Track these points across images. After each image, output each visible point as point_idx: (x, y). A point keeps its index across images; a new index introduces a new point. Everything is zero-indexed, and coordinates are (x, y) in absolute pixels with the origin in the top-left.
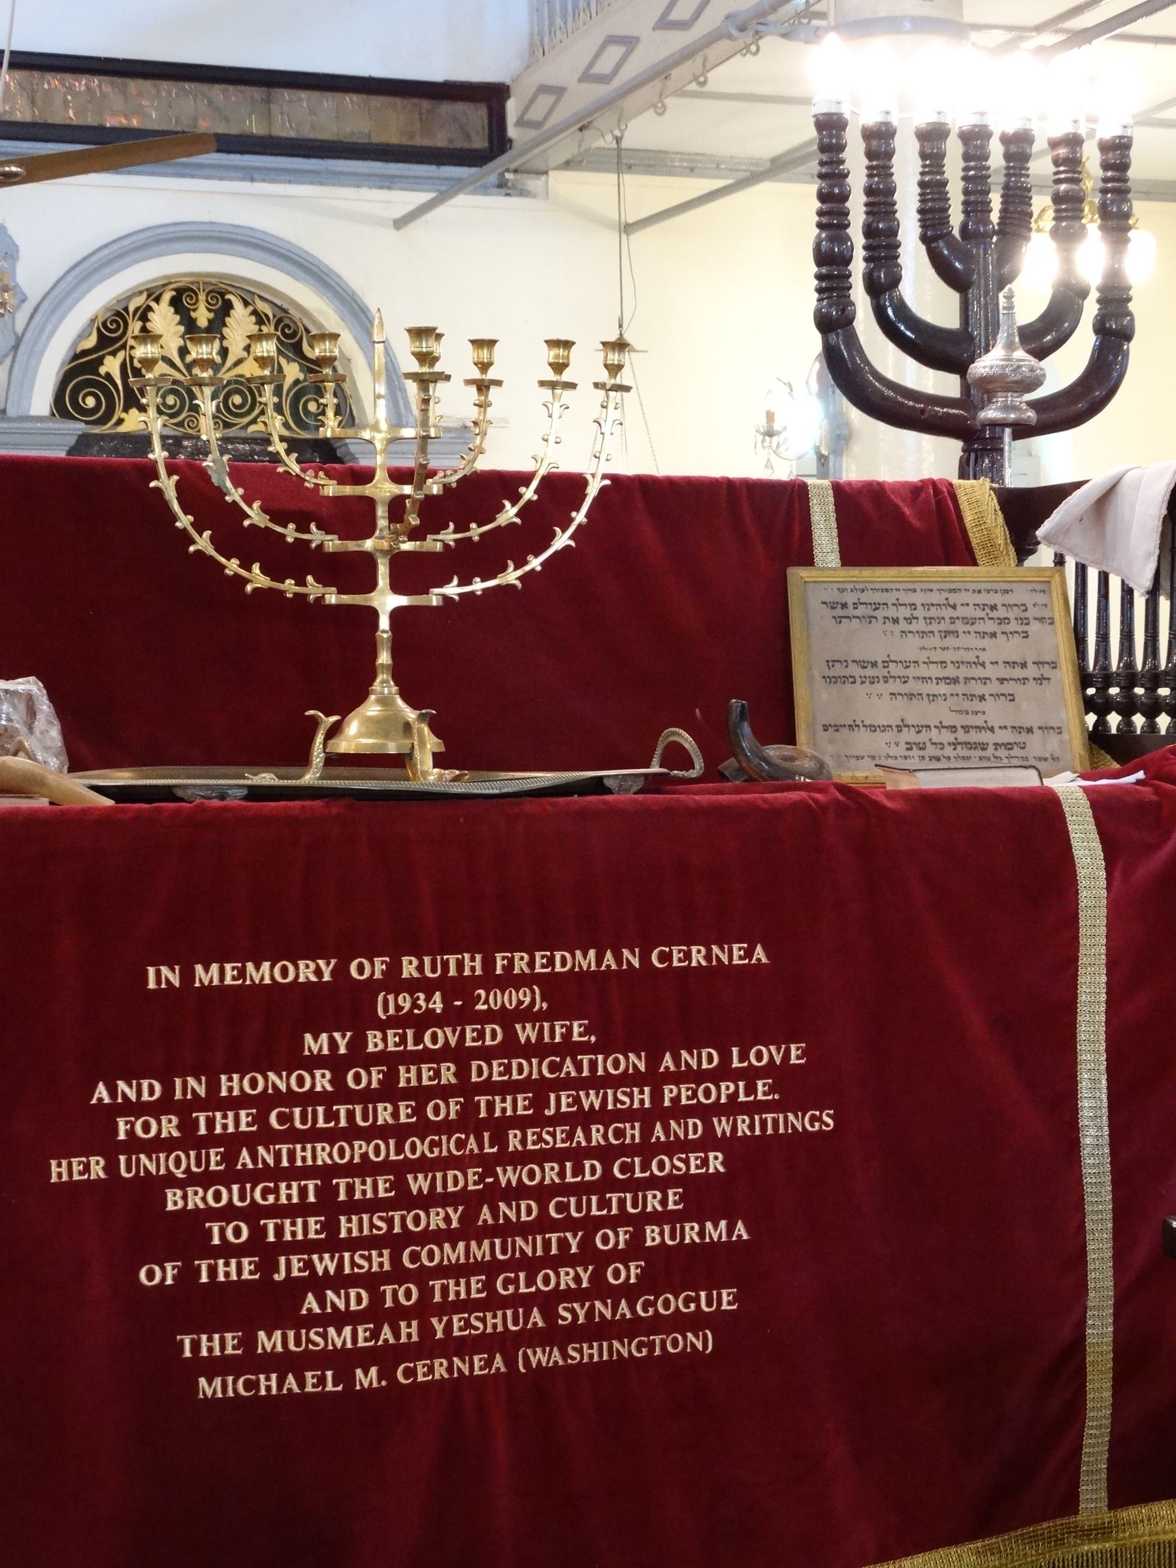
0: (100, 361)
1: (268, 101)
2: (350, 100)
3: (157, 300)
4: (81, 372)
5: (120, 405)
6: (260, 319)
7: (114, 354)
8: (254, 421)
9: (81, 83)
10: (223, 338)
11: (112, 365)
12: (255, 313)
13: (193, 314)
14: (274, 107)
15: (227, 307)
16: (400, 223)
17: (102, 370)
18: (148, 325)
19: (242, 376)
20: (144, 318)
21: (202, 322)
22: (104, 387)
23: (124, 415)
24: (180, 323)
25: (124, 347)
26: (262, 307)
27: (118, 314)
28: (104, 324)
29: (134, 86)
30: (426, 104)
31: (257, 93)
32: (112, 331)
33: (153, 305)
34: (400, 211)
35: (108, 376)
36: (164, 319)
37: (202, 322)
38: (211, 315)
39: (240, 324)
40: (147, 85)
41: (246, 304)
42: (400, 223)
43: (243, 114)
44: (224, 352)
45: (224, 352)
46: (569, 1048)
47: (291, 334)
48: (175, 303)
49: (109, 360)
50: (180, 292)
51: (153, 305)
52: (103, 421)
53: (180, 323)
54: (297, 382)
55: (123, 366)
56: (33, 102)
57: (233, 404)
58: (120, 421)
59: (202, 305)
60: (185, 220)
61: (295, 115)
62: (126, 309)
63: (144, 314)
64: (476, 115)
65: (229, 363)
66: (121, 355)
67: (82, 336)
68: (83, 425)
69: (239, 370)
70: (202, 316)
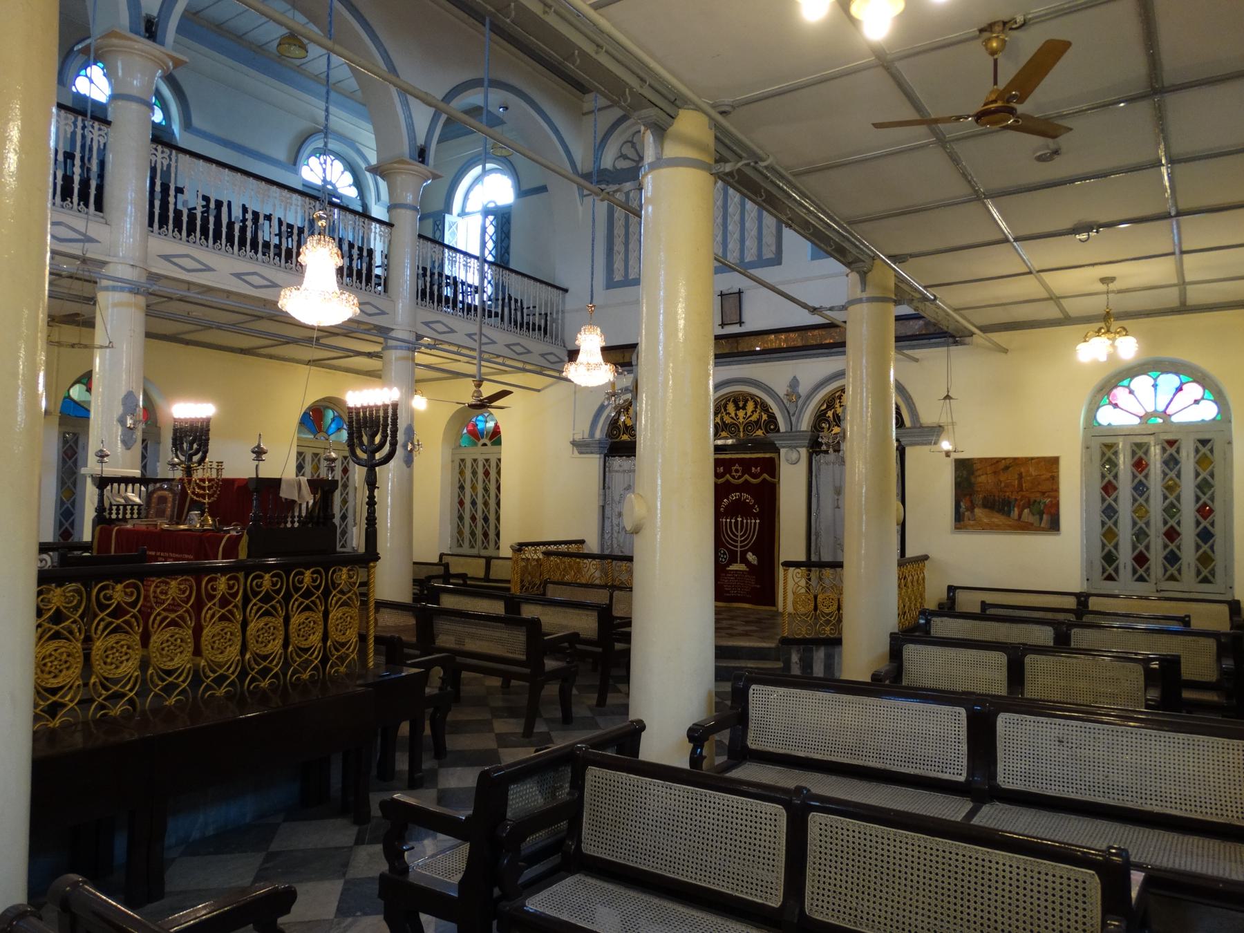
46: (293, 517)
64: (769, 253)
70: (741, 404)
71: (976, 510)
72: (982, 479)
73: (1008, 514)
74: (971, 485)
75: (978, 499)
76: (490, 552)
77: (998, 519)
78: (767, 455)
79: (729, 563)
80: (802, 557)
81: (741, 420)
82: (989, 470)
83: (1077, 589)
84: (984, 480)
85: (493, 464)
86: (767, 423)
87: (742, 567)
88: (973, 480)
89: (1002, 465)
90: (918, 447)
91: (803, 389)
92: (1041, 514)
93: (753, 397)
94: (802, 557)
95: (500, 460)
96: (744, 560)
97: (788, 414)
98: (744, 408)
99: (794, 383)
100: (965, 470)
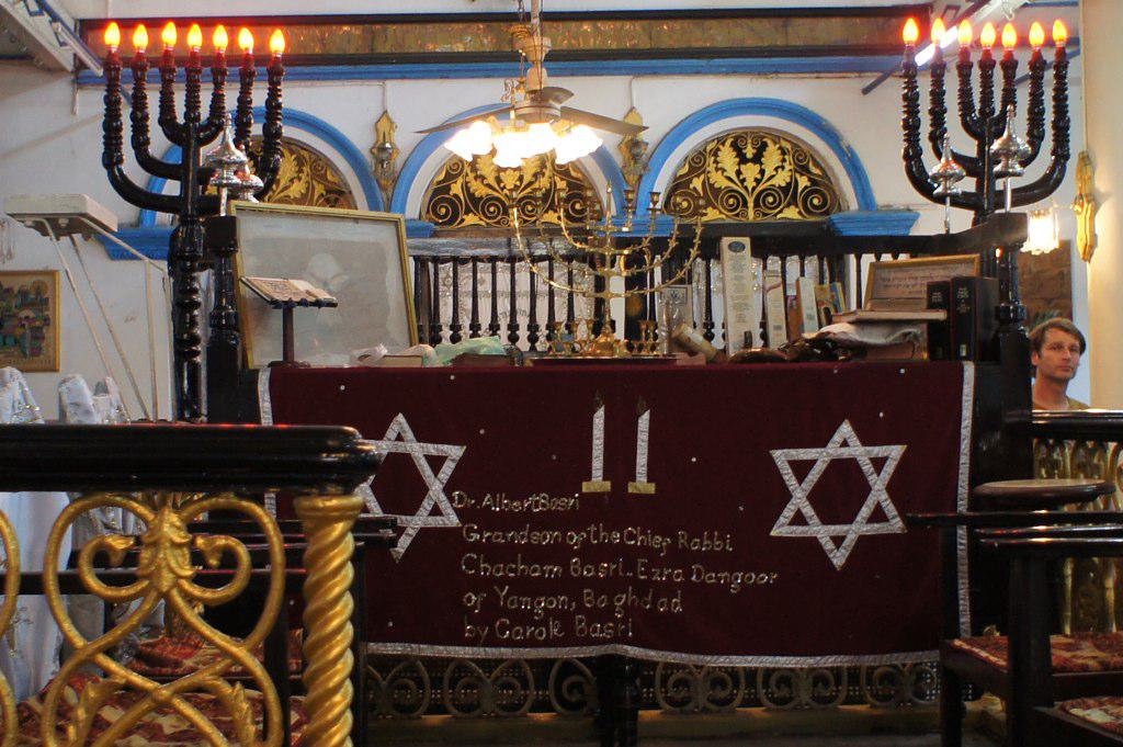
0: (690, 181)
1: (785, 26)
2: (836, 22)
3: (723, 144)
4: (679, 185)
5: (462, 212)
6: (783, 152)
7: (698, 176)
8: (781, 212)
9: (677, 25)
10: (761, 164)
11: (697, 183)
12: (780, 148)
13: (744, 151)
14: (790, 29)
15: (764, 145)
16: (866, 91)
17: (691, 186)
18: (718, 159)
19: (774, 185)
20: (716, 155)
21: (749, 155)
22: (453, 203)
23: (465, 217)
24: (736, 156)
25: (704, 172)
26: (784, 144)
27: (700, 153)
28: (693, 159)
29: (708, 23)
30: (881, 20)
31: (780, 22)
32: (697, 163)
33: (721, 147)
34: (868, 82)
35: (695, 189)
36: (728, 158)
37: (749, 155)
38: (755, 151)
39: (772, 157)
40: (714, 23)
41: (775, 143)
42: (866, 91)
43: (768, 34)
44: (762, 172)
45: (762, 172)
47: (802, 159)
48: (734, 146)
49: (695, 180)
50: (736, 138)
51: (721, 147)
52: (450, 222)
53: (736, 156)
54: (806, 187)
55: (704, 183)
56: (651, 38)
57: (811, 200)
58: (463, 220)
59: (748, 147)
60: (22, 269)
61: (801, 33)
62: (705, 150)
63: (715, 153)
65: (766, 176)
66: (702, 177)
67: (681, 166)
68: (724, 217)
69: (773, 182)
70: (750, 152)
81: (750, 184)
86: (809, 193)
93: (777, 137)
98: (757, 159)
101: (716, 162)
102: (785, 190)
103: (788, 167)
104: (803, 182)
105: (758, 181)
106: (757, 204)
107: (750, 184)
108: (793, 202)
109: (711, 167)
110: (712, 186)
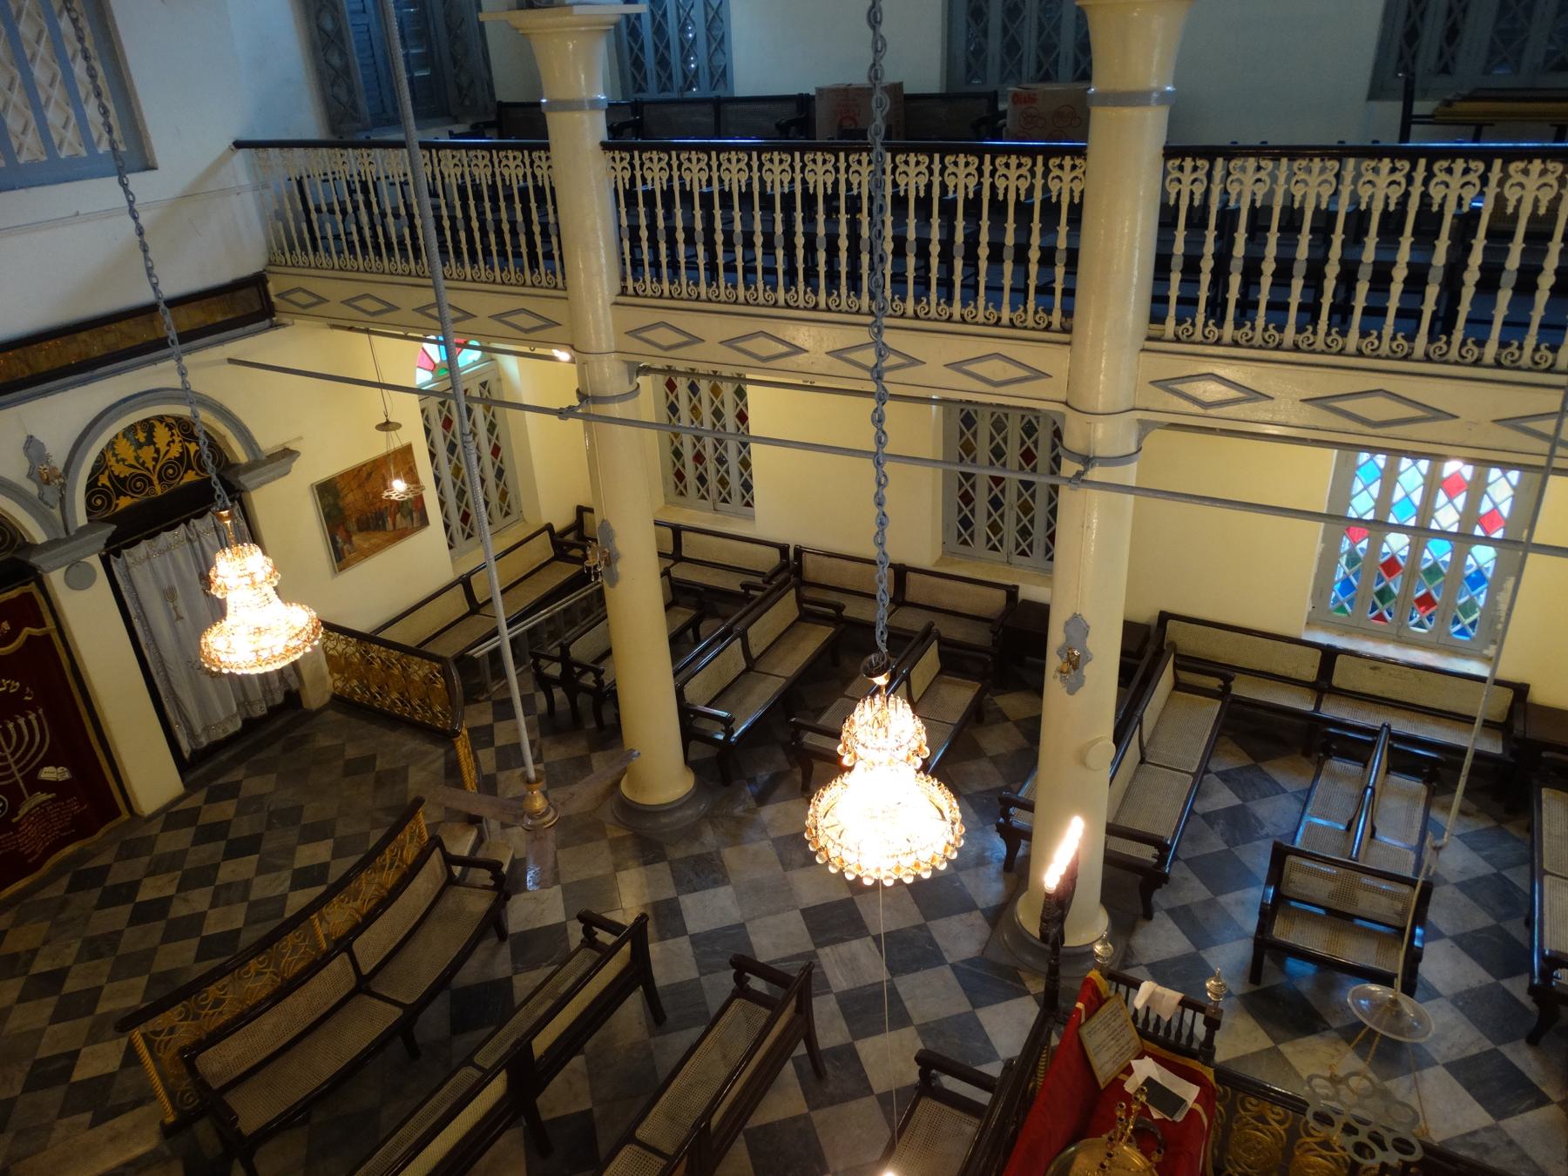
21: (142, 440)
37: (142, 440)
43: (43, 359)
45: (157, 451)
47: (185, 428)
71: (354, 538)
72: (350, 498)
73: (383, 528)
74: (341, 510)
75: (353, 526)
76: (721, 92)
77: (377, 538)
78: (13, 594)
79: (14, 811)
80: (1532, 558)
82: (354, 485)
83: (449, 575)
84: (351, 499)
85: (458, 538)
87: (41, 797)
88: (341, 504)
89: (364, 474)
90: (265, 487)
91: (58, 453)
92: (410, 513)
94: (1532, 558)
95: (450, 547)
96: (36, 785)
97: (34, 506)
99: (32, 446)
100: (328, 492)
101: (115, 455)
102: (180, 459)
103: (177, 439)
104: (193, 448)
105: (156, 460)
106: (160, 479)
107: (150, 465)
108: (190, 467)
109: (112, 461)
110: (117, 477)
